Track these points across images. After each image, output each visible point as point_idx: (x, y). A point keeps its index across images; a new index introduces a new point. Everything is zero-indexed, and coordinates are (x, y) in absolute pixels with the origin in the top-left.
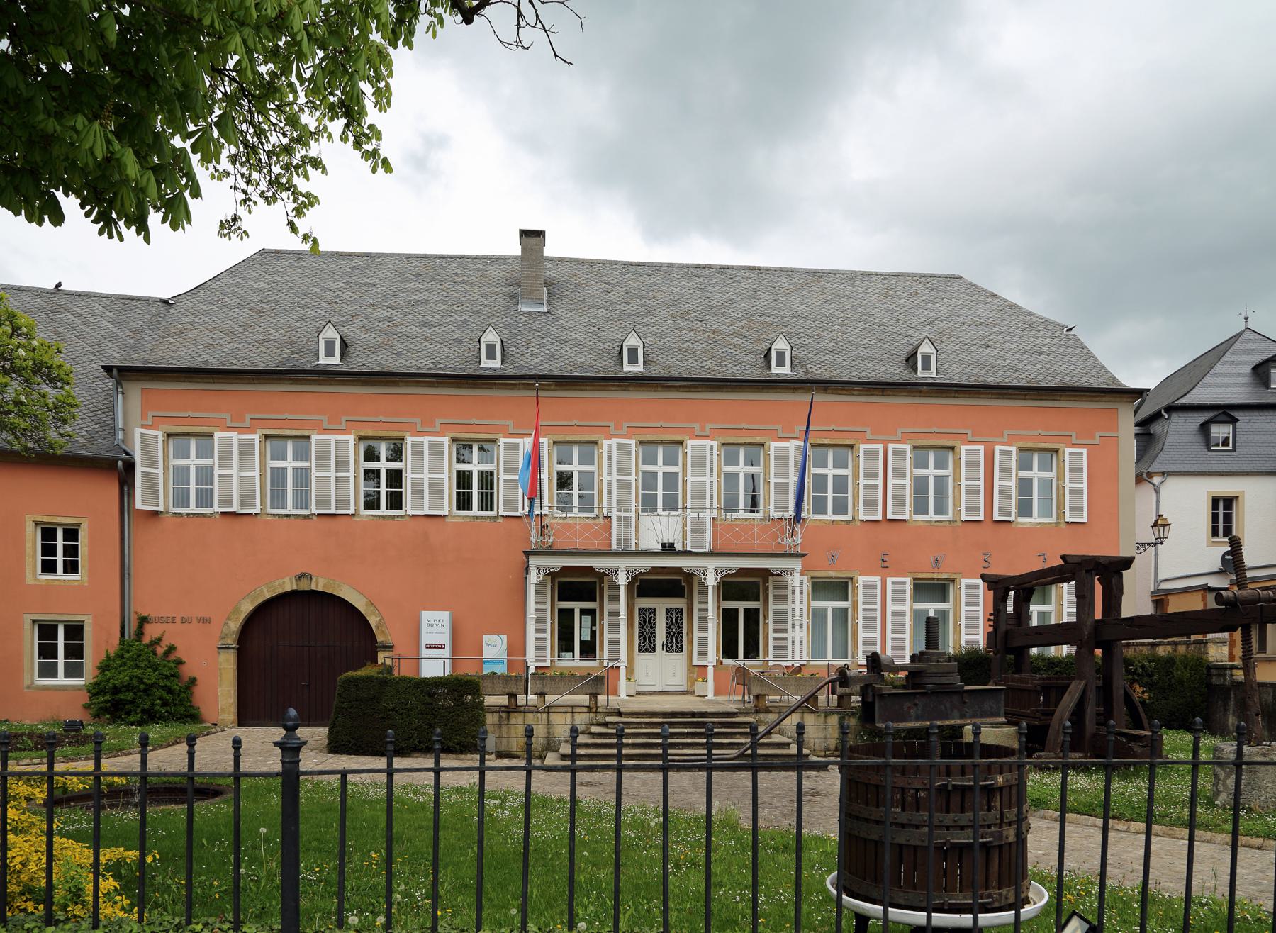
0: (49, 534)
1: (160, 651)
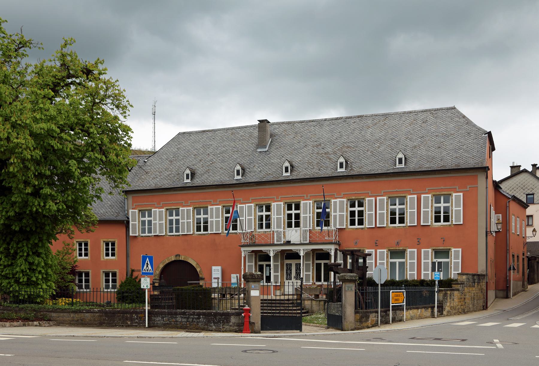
0: (107, 244)
1: (137, 281)
